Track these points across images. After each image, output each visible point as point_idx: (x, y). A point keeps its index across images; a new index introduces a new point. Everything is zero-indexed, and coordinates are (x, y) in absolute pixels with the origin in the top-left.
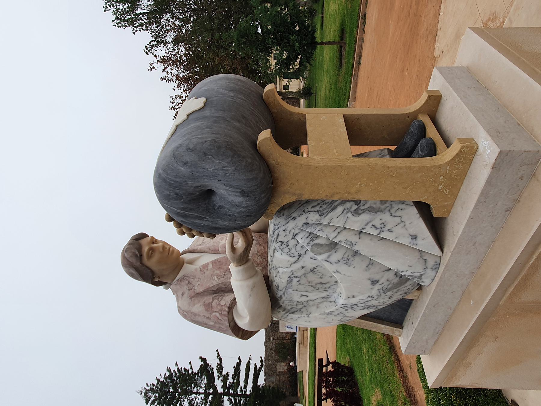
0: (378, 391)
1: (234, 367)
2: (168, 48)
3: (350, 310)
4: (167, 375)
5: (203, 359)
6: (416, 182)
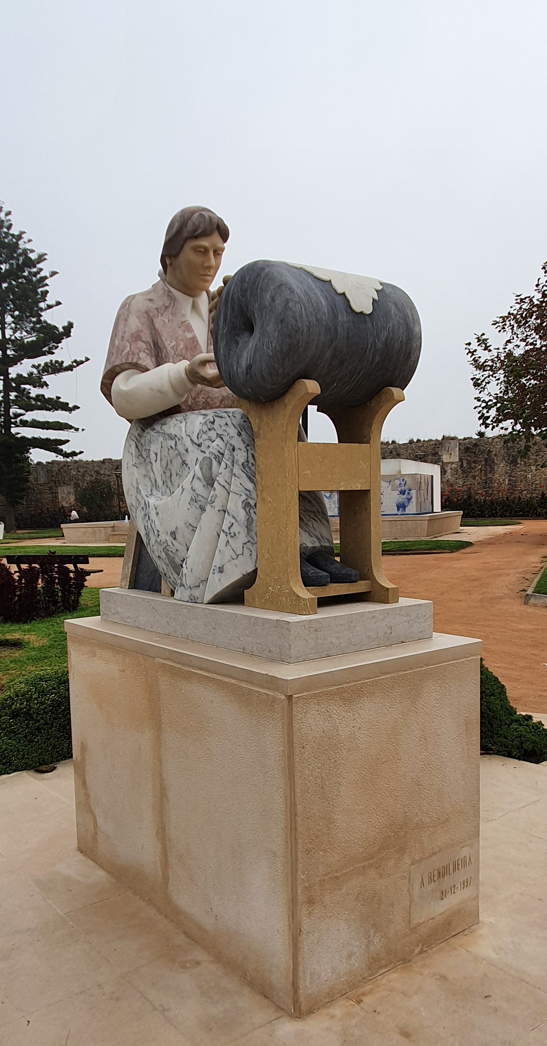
0: (46, 641)
1: (58, 398)
3: (143, 513)
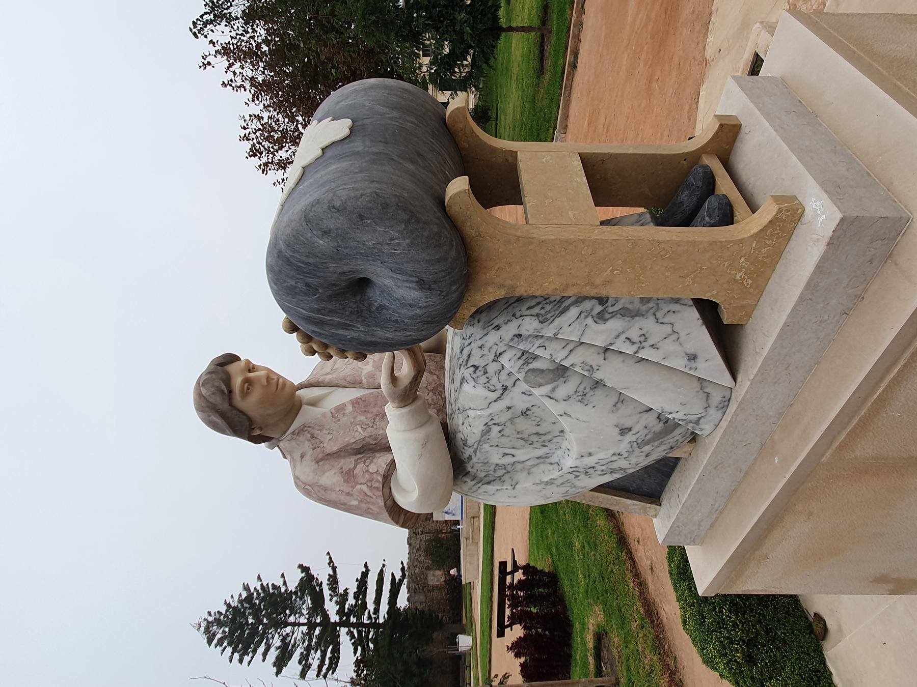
1: (357, 580)
2: (235, 27)
3: (582, 476)
4: (243, 597)
5: (305, 569)
6: (701, 268)
